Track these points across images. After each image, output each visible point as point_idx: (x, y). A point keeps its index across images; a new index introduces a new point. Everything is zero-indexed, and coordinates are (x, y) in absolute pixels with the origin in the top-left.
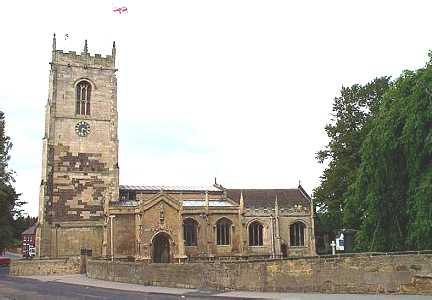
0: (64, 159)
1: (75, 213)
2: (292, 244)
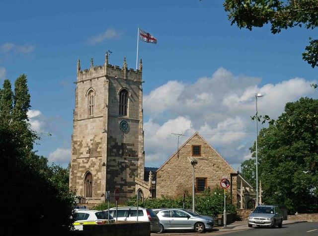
1: (119, 187)
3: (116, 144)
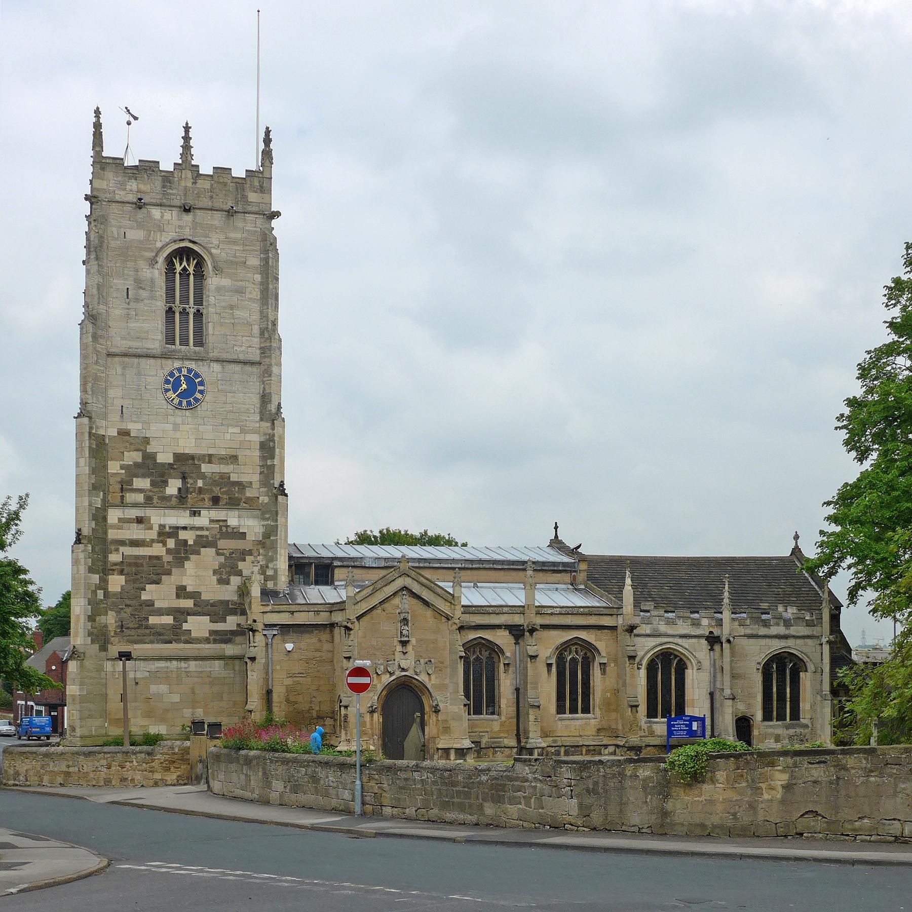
0: (134, 470)
1: (168, 620)
2: (767, 717)
3: (149, 458)
